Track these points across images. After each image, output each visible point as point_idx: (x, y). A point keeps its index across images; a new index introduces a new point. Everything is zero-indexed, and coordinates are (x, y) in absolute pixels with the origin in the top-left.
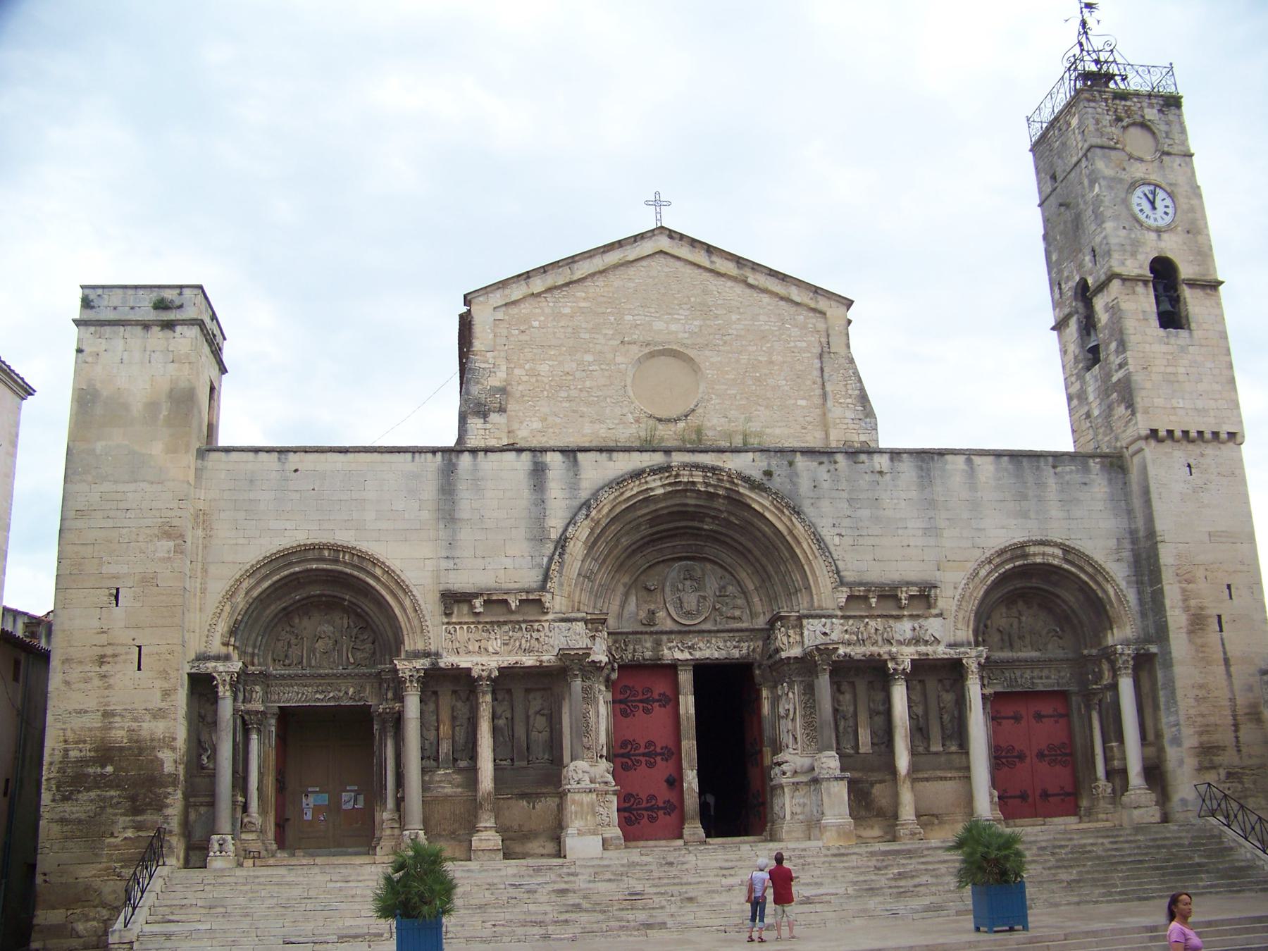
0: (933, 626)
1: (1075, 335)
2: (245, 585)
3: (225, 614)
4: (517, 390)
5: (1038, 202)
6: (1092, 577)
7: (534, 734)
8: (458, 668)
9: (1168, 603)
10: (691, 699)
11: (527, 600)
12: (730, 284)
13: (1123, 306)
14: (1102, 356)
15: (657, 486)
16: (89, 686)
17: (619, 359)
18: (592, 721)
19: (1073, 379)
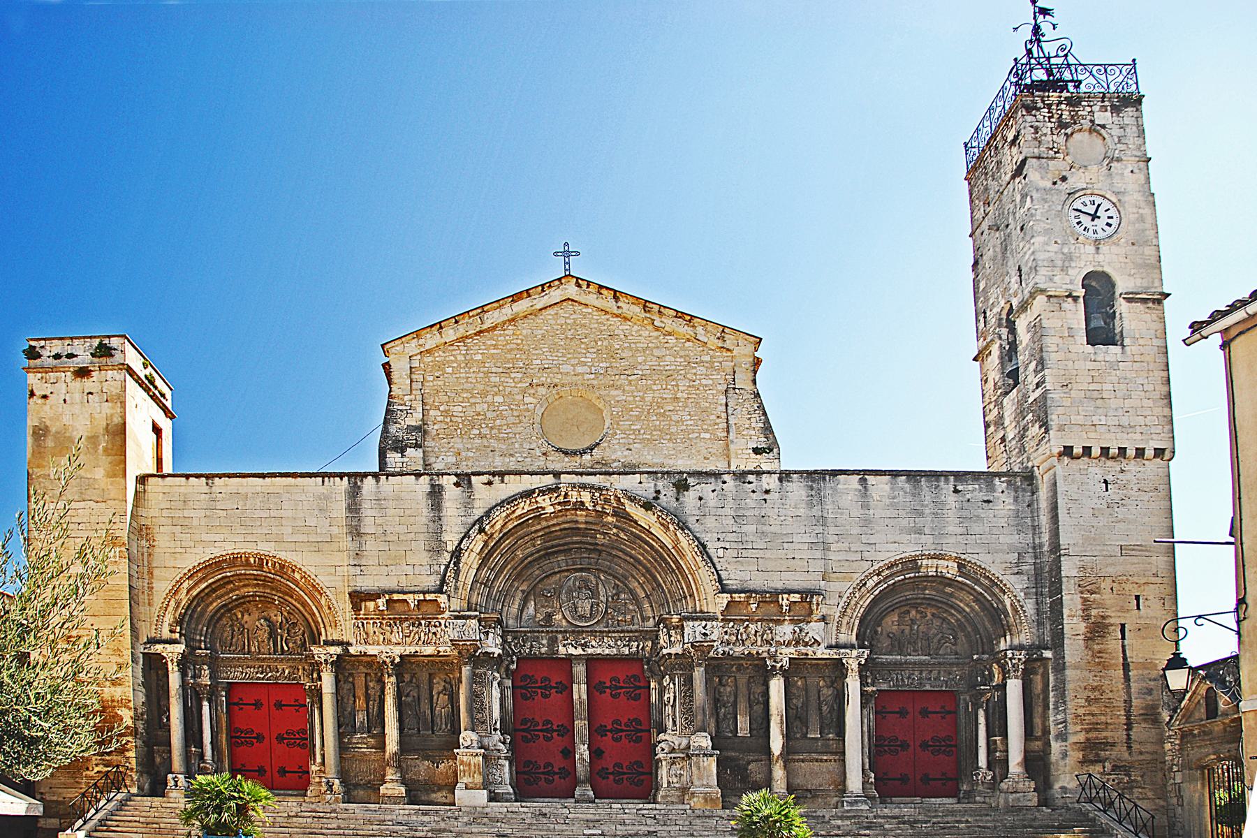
2: (186, 585)
3: (170, 609)
4: (432, 429)
6: (987, 589)
10: (584, 687)
18: (486, 701)
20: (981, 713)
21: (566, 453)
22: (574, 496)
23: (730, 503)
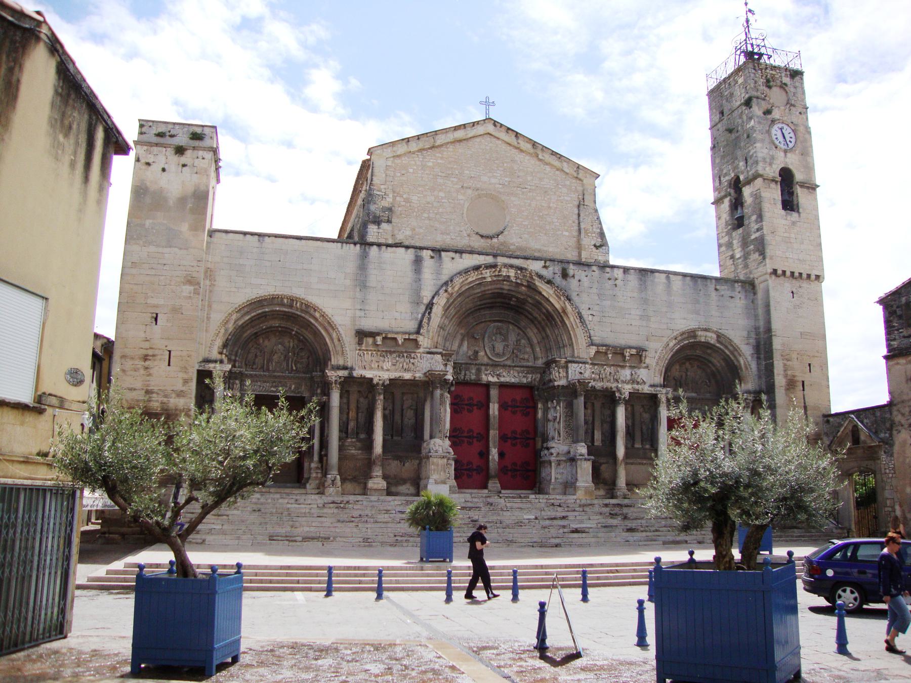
0: (643, 374)
1: (728, 209)
2: (234, 317)
4: (398, 210)
5: (709, 127)
6: (732, 353)
7: (406, 420)
8: (364, 377)
9: (776, 371)
11: (409, 339)
13: (763, 194)
14: (746, 222)
15: (488, 274)
16: (137, 373)
17: (460, 197)
18: (442, 415)
19: (724, 234)
21: (482, 236)
22: (504, 272)
23: (596, 285)
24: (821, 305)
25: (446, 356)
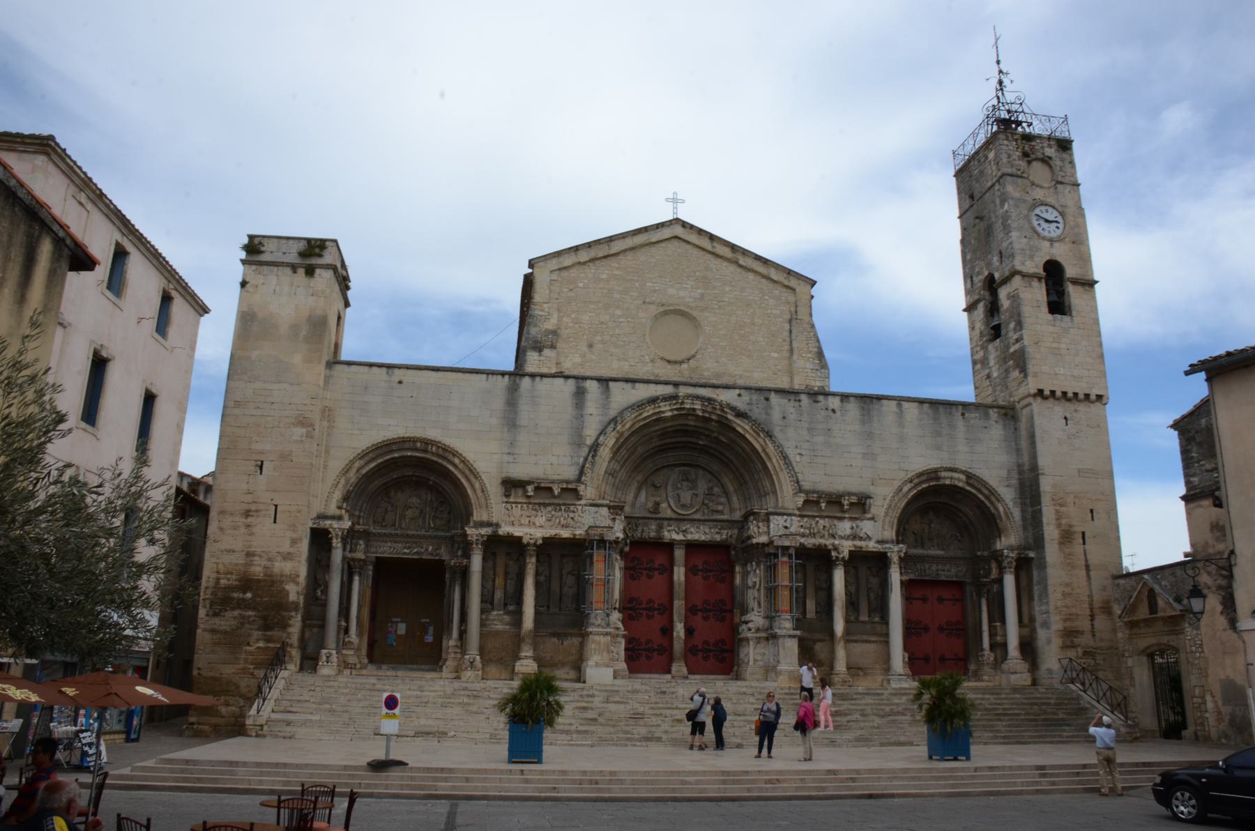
0: (867, 527)
2: (357, 465)
3: (340, 486)
4: (564, 333)
6: (987, 497)
7: (565, 589)
9: (1045, 520)
12: (725, 264)
13: (1022, 295)
14: (1003, 332)
15: (667, 409)
17: (641, 314)
20: (984, 602)
21: (669, 362)
24: (1106, 432)
25: (616, 509)
